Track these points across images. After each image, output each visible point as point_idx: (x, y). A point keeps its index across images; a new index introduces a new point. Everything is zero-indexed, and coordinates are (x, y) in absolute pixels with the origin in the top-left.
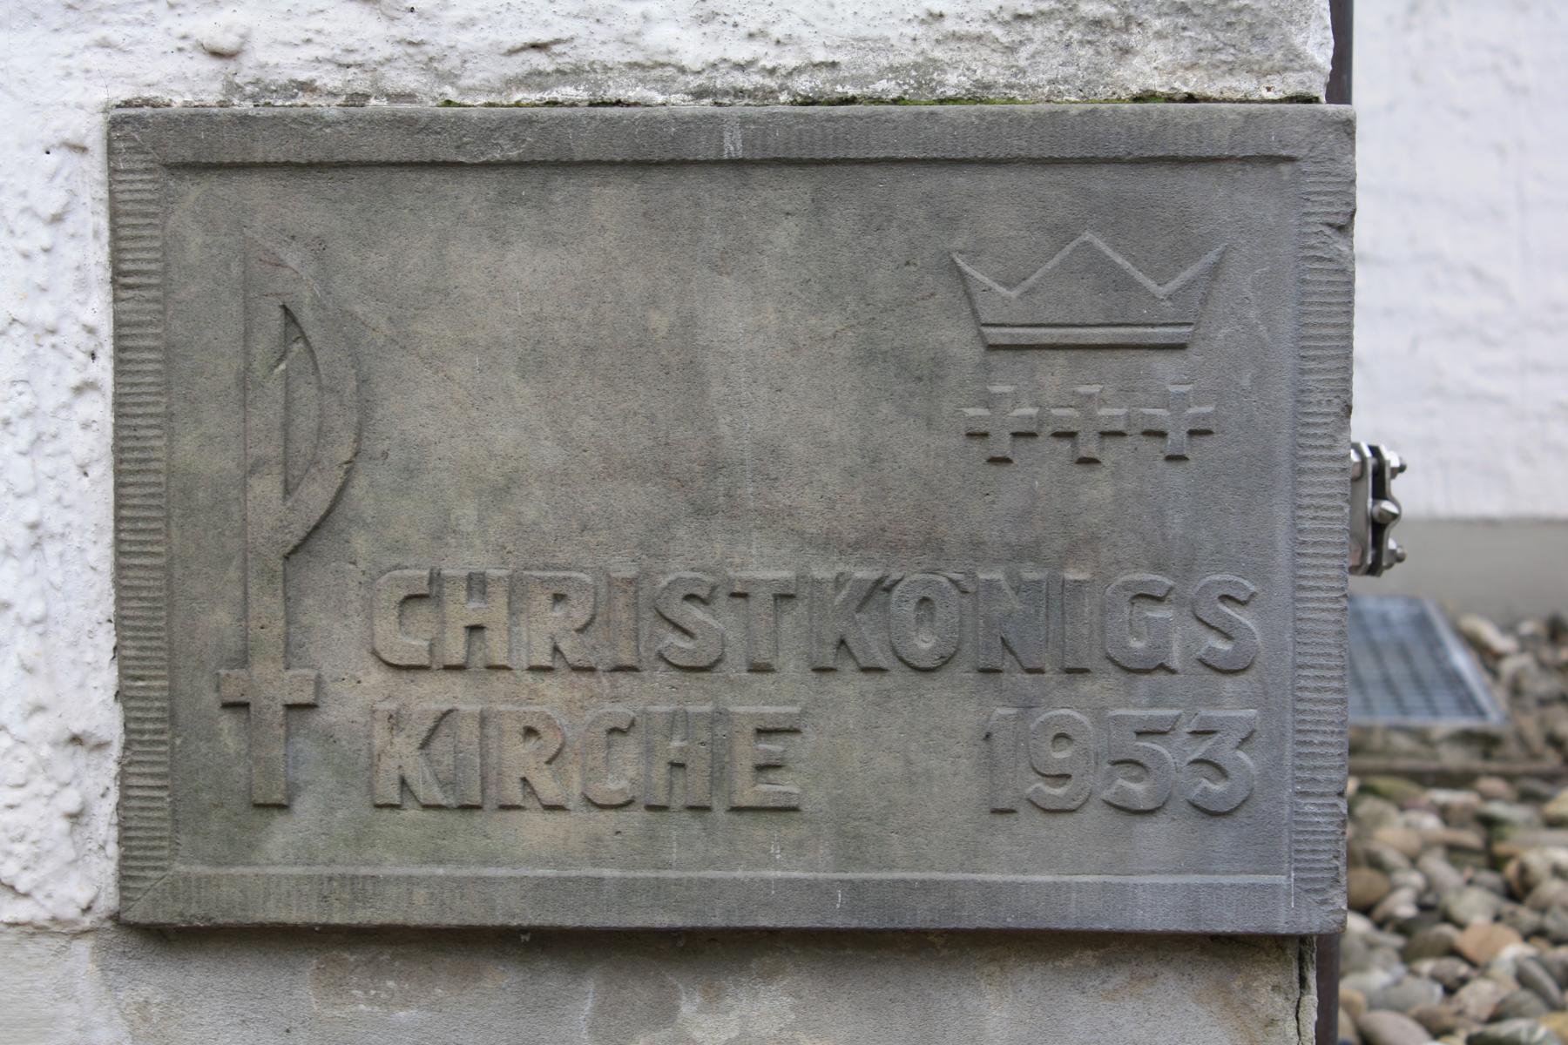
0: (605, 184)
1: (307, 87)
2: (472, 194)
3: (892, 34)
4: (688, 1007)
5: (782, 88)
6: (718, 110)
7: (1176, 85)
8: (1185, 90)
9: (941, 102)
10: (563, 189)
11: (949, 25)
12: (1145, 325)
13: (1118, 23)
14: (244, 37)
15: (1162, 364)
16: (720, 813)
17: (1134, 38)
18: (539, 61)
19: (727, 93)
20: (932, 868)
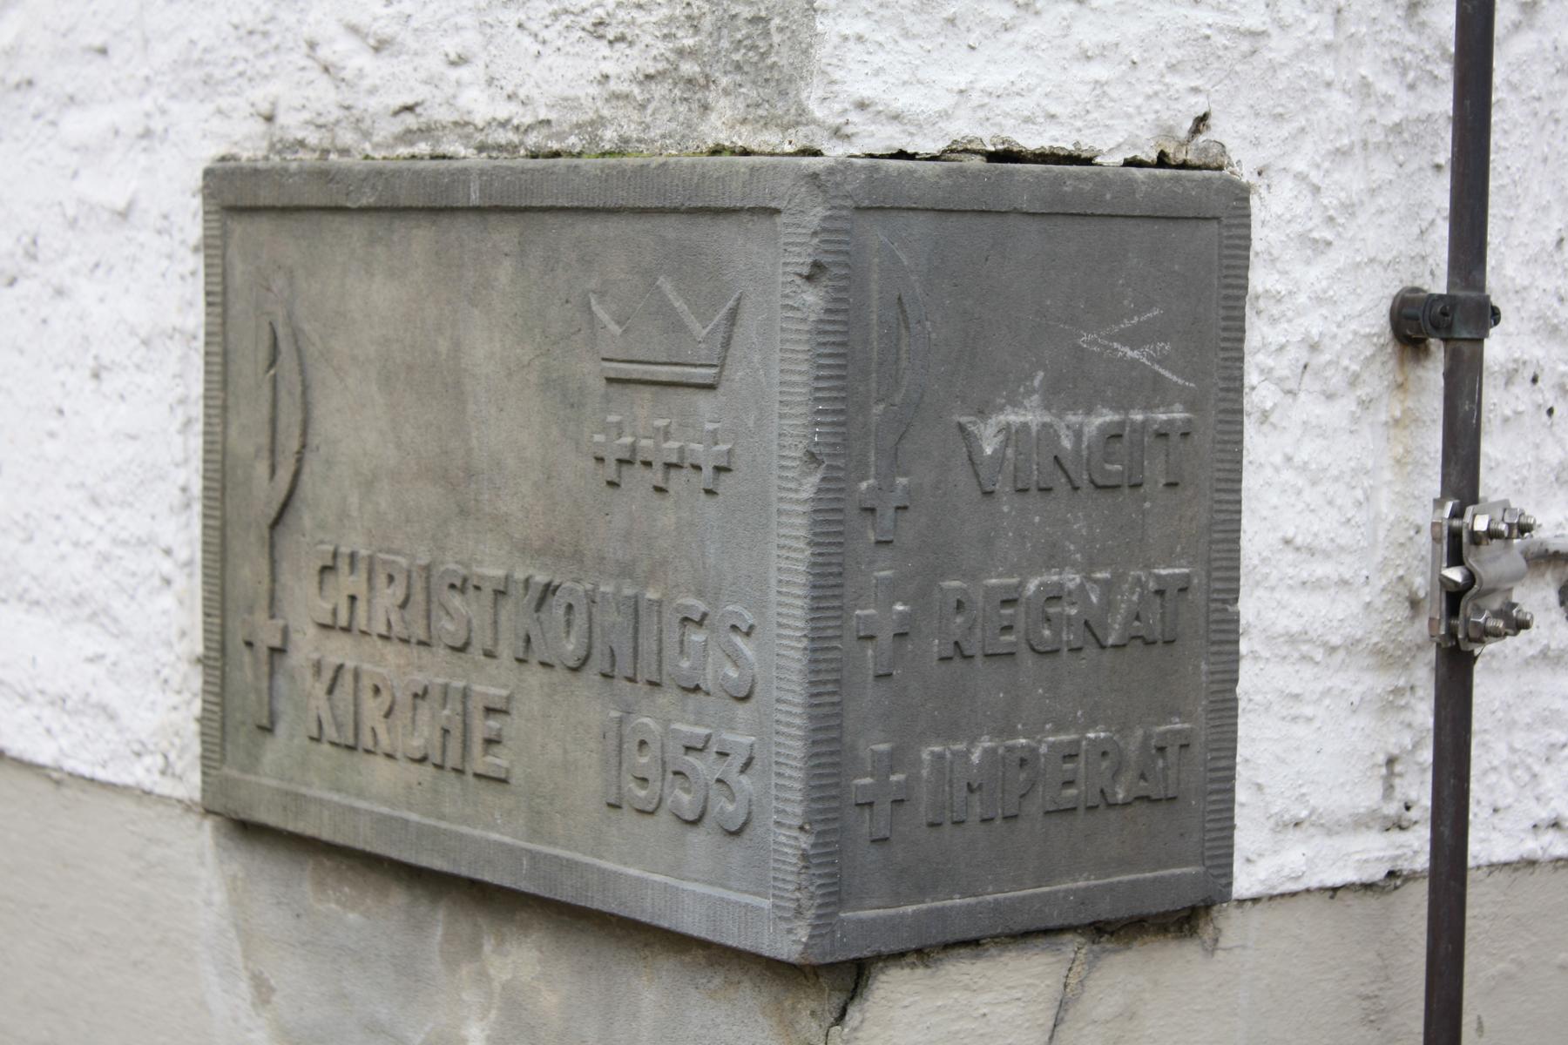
0: (418, 227)
1: (301, 143)
2: (356, 231)
3: (581, 94)
4: (488, 946)
5: (522, 143)
6: (493, 162)
7: (735, 139)
8: (740, 143)
9: (603, 154)
10: (400, 226)
11: (613, 85)
12: (676, 364)
13: (702, 81)
14: (274, 104)
15: (703, 401)
16: (947, 825)
17: (711, 96)
18: (410, 120)
19: (494, 148)
20: (576, 849)
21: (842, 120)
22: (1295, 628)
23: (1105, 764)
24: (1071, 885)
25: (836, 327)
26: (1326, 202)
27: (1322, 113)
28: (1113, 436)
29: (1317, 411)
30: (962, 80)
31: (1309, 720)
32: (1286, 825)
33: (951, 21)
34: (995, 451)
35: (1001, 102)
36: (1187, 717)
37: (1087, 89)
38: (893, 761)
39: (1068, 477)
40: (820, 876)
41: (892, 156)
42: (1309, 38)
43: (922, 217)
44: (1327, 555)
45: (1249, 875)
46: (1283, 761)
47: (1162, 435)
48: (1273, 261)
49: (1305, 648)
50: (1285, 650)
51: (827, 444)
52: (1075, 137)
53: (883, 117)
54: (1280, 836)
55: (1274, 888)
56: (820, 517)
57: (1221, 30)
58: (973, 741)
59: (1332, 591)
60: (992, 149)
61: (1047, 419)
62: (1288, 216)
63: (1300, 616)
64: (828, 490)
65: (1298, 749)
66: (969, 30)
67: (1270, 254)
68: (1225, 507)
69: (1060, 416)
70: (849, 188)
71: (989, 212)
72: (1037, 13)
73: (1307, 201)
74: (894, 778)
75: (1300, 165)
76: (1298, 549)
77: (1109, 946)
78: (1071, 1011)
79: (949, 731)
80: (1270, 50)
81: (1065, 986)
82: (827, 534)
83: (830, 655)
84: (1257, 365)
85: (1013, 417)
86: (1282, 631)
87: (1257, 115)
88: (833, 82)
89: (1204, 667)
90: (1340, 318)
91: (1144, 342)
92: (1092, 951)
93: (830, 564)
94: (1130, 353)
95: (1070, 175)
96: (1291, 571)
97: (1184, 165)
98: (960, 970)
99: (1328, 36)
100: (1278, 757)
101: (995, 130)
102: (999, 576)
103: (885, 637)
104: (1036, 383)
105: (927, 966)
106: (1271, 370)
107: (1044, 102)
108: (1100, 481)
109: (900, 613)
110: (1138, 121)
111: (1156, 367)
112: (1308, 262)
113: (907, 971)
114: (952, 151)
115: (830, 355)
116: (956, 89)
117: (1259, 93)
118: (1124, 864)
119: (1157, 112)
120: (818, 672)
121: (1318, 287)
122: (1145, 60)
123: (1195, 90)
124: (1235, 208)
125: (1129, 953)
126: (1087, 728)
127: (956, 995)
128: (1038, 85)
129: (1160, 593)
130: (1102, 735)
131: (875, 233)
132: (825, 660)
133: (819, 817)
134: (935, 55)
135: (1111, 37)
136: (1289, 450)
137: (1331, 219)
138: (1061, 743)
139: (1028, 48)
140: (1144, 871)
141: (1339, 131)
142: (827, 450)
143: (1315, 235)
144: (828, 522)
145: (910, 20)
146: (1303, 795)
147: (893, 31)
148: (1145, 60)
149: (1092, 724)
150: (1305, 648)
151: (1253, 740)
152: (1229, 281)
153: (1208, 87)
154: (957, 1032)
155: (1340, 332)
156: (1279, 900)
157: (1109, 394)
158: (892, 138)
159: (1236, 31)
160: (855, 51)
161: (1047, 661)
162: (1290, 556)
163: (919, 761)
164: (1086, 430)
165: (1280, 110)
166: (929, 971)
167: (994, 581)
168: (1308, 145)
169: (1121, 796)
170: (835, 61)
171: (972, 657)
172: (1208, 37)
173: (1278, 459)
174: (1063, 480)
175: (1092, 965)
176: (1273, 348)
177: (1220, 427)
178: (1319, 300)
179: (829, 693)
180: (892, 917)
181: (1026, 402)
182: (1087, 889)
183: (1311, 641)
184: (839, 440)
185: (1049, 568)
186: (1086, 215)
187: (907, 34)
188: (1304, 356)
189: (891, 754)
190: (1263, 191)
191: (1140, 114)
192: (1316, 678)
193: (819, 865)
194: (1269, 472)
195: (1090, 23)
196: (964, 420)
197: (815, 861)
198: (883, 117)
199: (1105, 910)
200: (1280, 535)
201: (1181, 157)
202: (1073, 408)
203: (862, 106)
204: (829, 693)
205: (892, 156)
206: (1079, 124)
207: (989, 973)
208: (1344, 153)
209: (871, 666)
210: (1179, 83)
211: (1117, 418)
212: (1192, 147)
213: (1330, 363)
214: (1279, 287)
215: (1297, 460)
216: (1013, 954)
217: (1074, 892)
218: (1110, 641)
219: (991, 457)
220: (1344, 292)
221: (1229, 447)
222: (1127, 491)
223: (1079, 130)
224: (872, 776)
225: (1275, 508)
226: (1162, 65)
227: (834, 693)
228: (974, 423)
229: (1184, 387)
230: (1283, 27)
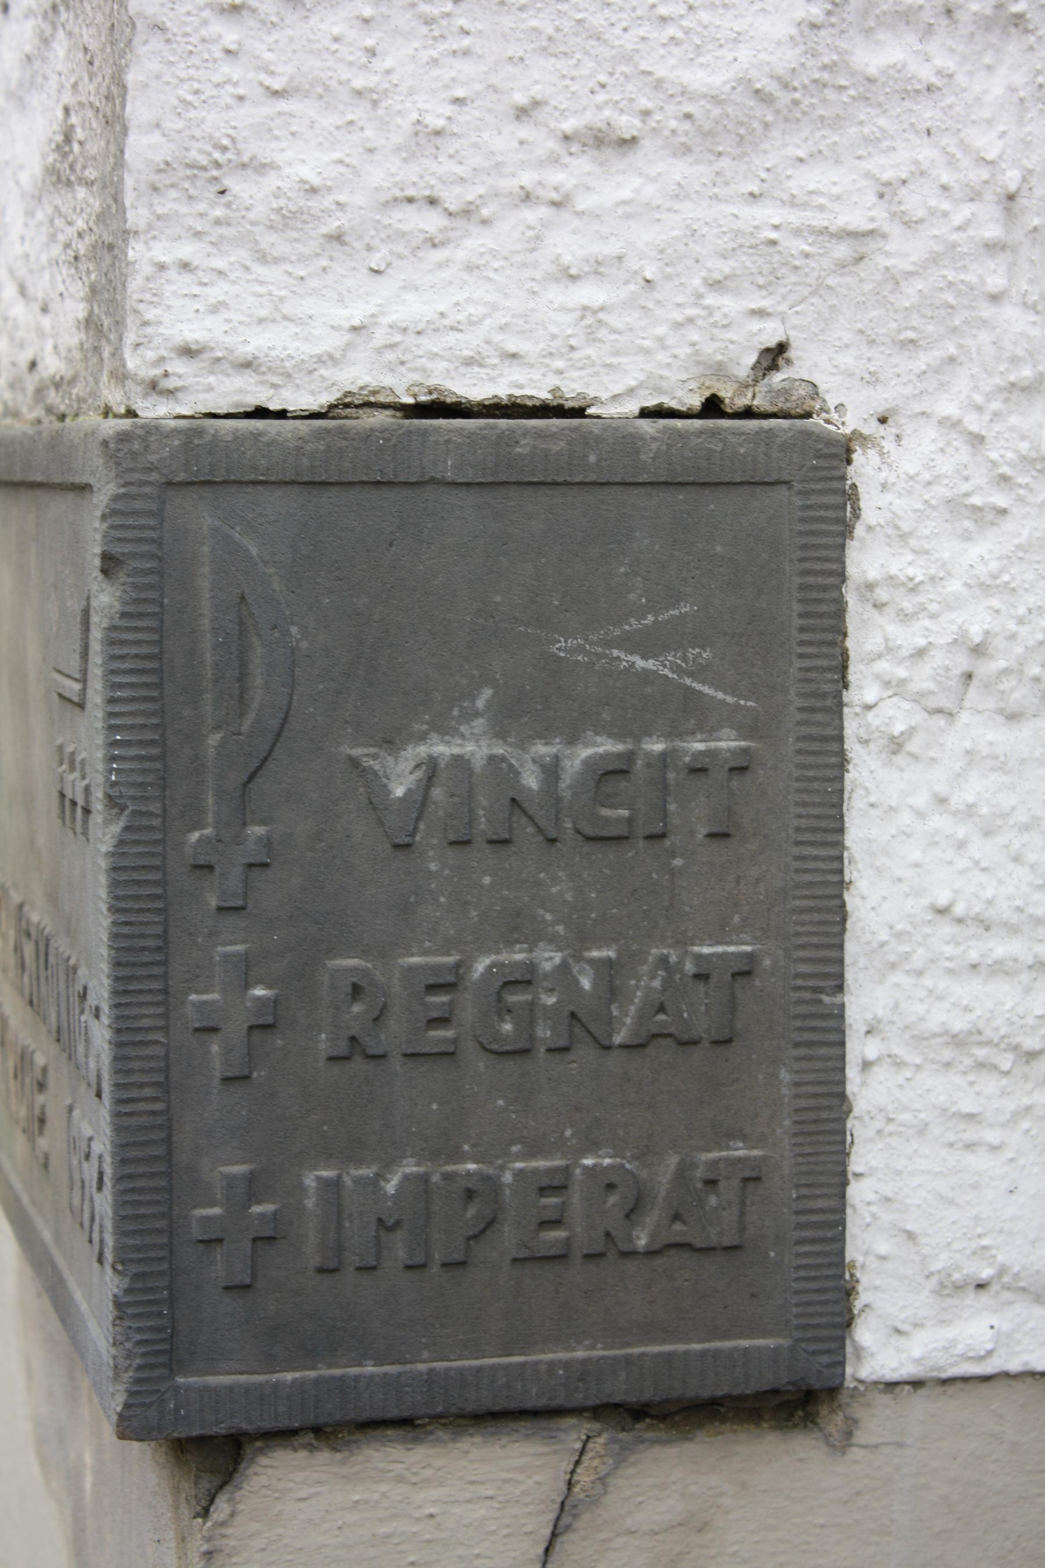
21: (157, 372)
22: (959, 1024)
23: (613, 1199)
24: (563, 1355)
25: (140, 636)
26: (994, 455)
27: (984, 337)
28: (611, 773)
29: (990, 737)
30: (357, 314)
31: (995, 1149)
32: (959, 1288)
33: (338, 238)
34: (409, 792)
35: (423, 340)
36: (760, 1141)
37: (569, 318)
38: (253, 1187)
39: (537, 825)
40: (139, 1330)
41: (247, 415)
42: (955, 236)
43: (278, 493)
44: (1013, 930)
45: (898, 1350)
46: (951, 1202)
47: (697, 770)
48: (903, 537)
49: (981, 1053)
50: (947, 1054)
51: (132, 785)
52: (553, 381)
53: (226, 365)
54: (949, 1301)
55: (940, 1369)
56: (124, 876)
57: (797, 232)
58: (388, 1165)
59: (1025, 977)
60: (411, 401)
61: (499, 750)
62: (927, 476)
63: (967, 1009)
64: (136, 842)
65: (975, 1187)
66: (369, 248)
67: (897, 527)
68: (812, 865)
69: (522, 745)
70: (153, 458)
71: (390, 483)
72: (484, 222)
73: (964, 453)
74: (257, 1209)
75: (948, 407)
76: (960, 921)
77: (650, 1435)
78: (586, 1517)
79: (352, 1151)
80: (888, 254)
81: (570, 1484)
82: (137, 898)
83: (147, 1051)
84: (877, 677)
85: (442, 749)
86: (938, 1030)
87: (871, 342)
88: (146, 324)
89: (785, 1075)
90: (1022, 610)
91: (666, 648)
92: (613, 1441)
93: (142, 936)
94: (640, 663)
95: (526, 433)
96: (949, 950)
97: (748, 413)
98: (388, 1460)
99: (993, 232)
100: (941, 1197)
101: (416, 377)
102: (425, 953)
103: (236, 1028)
104: (480, 703)
105: (335, 1449)
106: (902, 682)
107: (498, 338)
108: (589, 831)
109: (259, 999)
110: (662, 357)
111: (688, 681)
112: (967, 537)
113: (302, 1454)
114: (347, 406)
115: (132, 672)
116: (346, 325)
117: (873, 314)
118: (650, 1331)
119: (693, 344)
120: (130, 1072)
121: (981, 570)
122: (668, 277)
123: (760, 313)
124: (815, 468)
125: (688, 1446)
126: (584, 1152)
127: (384, 1488)
128: (489, 315)
129: (701, 977)
130: (607, 1161)
131: (201, 516)
132: (138, 1058)
133: (135, 1256)
134: (313, 283)
135: (612, 248)
136: (941, 789)
137: (1005, 478)
138: (535, 1171)
139: (470, 268)
140: (689, 1341)
141: (1015, 360)
142: (132, 792)
143: (976, 500)
144: (138, 883)
145: (267, 240)
146: (985, 1248)
147: (243, 254)
148: (668, 277)
149: (593, 1147)
150: (981, 1053)
151: (898, 1173)
152: (808, 565)
153: (783, 308)
154: (388, 1536)
155: (1023, 631)
156: (959, 1385)
157: (606, 716)
158: (241, 391)
159: (824, 231)
160: (184, 282)
161: (510, 1065)
162: (947, 929)
163: (303, 1190)
164: (567, 764)
165: (910, 335)
166: (339, 1456)
167: (415, 960)
168: (962, 382)
169: (642, 1242)
170: (148, 296)
171: (383, 1056)
172: (773, 243)
173: (921, 800)
174: (530, 829)
175: (620, 1461)
176: (905, 652)
177: (800, 759)
178: (985, 587)
179: (146, 1099)
180: (260, 1386)
181: (463, 728)
182: (585, 1362)
183: (988, 1043)
184: (150, 778)
185: (510, 944)
186: (555, 484)
187: (263, 258)
188: (962, 662)
189: (251, 1179)
190: (888, 445)
191: (664, 347)
192: (1004, 1093)
193: (135, 1316)
194: (906, 818)
195: (574, 232)
196: (356, 752)
197: (130, 1311)
198: (226, 365)
199: (618, 1389)
200: (925, 901)
201: (741, 402)
202: (545, 735)
203: (188, 352)
204: (146, 1099)
205: (247, 415)
206: (559, 364)
207: (438, 1463)
208: (1024, 389)
209: (217, 1065)
210: (729, 304)
211: (620, 747)
212: (762, 388)
213: (1005, 672)
214: (911, 572)
215: (956, 802)
216: (477, 1439)
217: (567, 1365)
218: (618, 1039)
219: (401, 800)
220: (1030, 576)
221: (816, 785)
222: (641, 843)
223: (559, 372)
224: (222, 1206)
225: (917, 865)
226: (697, 282)
227: (155, 1099)
228: (375, 757)
229: (737, 706)
230: (910, 224)
